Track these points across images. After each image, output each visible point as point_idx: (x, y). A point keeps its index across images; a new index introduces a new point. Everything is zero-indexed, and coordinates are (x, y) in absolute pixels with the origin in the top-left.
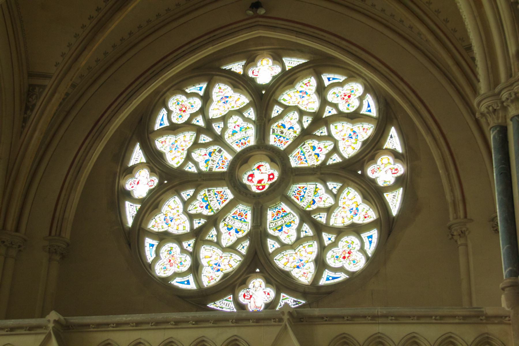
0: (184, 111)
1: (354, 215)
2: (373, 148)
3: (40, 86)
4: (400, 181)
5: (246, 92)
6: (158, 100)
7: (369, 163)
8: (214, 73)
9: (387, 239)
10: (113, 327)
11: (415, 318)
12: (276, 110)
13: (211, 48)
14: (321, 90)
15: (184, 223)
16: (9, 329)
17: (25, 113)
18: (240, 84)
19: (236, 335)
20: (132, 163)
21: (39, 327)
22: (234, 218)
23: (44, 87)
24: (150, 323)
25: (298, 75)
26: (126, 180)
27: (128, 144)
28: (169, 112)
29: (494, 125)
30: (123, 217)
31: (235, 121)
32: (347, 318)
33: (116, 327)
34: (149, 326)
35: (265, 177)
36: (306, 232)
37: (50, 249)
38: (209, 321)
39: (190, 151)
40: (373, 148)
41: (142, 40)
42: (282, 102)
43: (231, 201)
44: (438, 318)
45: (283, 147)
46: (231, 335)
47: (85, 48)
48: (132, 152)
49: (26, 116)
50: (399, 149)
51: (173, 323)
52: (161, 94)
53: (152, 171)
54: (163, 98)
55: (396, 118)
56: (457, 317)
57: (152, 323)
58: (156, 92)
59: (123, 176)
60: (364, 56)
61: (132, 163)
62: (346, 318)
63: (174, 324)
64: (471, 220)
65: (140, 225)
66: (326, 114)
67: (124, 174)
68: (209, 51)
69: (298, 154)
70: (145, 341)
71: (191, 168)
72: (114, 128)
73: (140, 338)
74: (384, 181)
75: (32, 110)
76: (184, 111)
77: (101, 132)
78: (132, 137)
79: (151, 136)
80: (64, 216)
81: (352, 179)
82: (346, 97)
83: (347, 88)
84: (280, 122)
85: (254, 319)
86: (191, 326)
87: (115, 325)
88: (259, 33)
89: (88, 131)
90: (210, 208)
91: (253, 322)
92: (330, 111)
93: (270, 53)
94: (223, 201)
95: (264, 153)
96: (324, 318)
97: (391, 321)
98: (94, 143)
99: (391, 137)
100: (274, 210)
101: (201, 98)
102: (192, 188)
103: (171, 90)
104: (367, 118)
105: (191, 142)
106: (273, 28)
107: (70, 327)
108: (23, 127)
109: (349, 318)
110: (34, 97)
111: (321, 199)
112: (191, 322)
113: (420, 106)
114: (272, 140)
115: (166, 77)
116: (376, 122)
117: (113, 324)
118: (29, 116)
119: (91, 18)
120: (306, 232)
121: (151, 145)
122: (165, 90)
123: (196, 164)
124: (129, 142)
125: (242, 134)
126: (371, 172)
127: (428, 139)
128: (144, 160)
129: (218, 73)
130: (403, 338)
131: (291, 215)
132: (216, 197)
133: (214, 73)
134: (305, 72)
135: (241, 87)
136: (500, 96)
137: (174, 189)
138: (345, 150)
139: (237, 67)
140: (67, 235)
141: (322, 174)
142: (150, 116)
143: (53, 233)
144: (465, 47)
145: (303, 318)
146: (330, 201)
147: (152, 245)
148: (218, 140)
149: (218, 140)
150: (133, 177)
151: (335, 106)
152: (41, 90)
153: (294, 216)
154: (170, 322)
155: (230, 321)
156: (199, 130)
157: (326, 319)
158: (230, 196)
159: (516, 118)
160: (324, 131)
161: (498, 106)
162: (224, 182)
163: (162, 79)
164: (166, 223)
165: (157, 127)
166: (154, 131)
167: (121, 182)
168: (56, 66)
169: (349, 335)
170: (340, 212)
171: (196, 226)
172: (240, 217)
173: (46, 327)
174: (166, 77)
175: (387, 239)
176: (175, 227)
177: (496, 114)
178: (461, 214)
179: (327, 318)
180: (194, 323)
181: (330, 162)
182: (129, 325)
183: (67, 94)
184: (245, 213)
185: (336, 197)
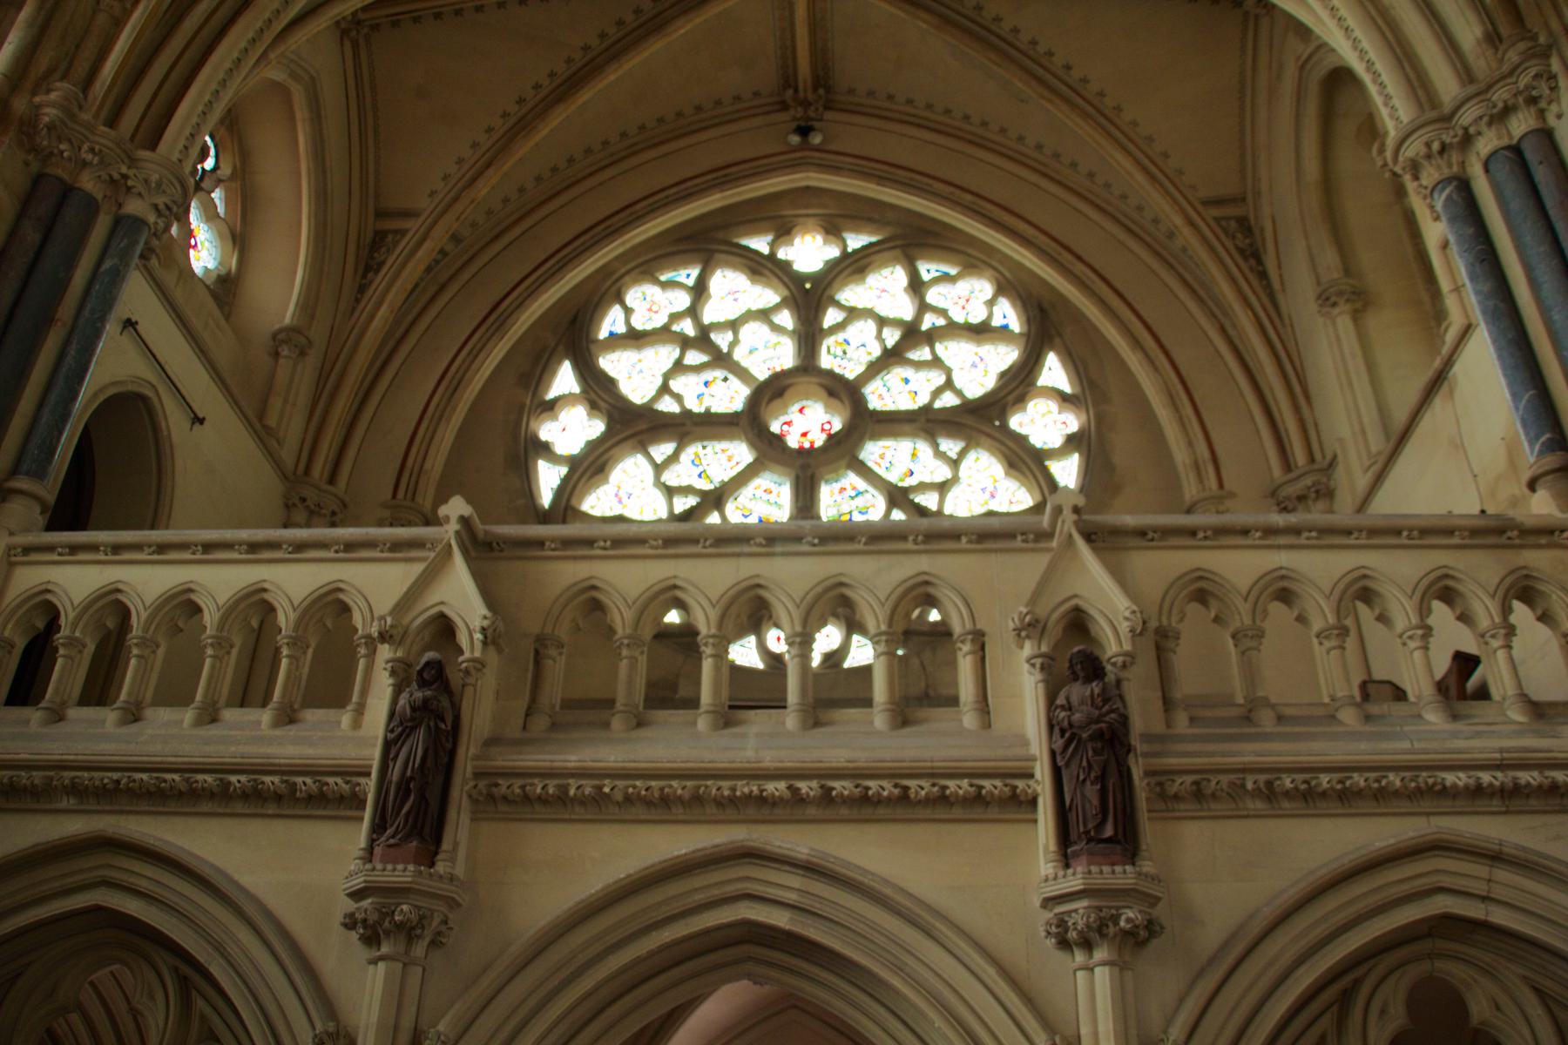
0: (656, 312)
3: (396, 232)
4: (1073, 442)
5: (776, 281)
10: (605, 548)
11: (1364, 534)
12: (831, 317)
13: (718, 196)
14: (916, 286)
17: (364, 276)
20: (552, 394)
21: (418, 544)
23: (403, 233)
24: (702, 541)
26: (543, 421)
27: (548, 360)
28: (628, 311)
29: (1440, 178)
30: (534, 487)
31: (753, 332)
32: (1205, 532)
39: (667, 377)
41: (591, 175)
42: (843, 302)
43: (749, 466)
44: (1415, 533)
45: (851, 375)
46: (910, 572)
47: (488, 165)
48: (554, 373)
49: (364, 281)
50: (1067, 388)
53: (593, 407)
54: (618, 284)
55: (1060, 335)
56: (1457, 533)
57: (706, 540)
61: (552, 394)
62: (1201, 535)
64: (1232, 495)
65: (568, 500)
66: (925, 326)
67: (539, 410)
68: (713, 202)
71: (667, 405)
72: (529, 317)
75: (377, 271)
76: (656, 312)
77: (504, 321)
78: (557, 346)
79: (593, 347)
80: (422, 467)
84: (840, 337)
86: (806, 548)
87: (609, 543)
88: (808, 178)
91: (970, 542)
92: (928, 321)
97: (1306, 542)
98: (488, 340)
102: (668, 440)
104: (1003, 333)
107: (495, 544)
108: (358, 301)
109: (1209, 533)
110: (384, 250)
113: (1115, 302)
114: (826, 361)
116: (1023, 341)
117: (605, 541)
118: (371, 282)
119: (505, 115)
123: (678, 398)
126: (1017, 422)
127: (1133, 360)
128: (576, 389)
130: (1340, 580)
134: (886, 255)
136: (1454, 122)
139: (760, 244)
141: (928, 421)
142: (592, 316)
145: (1096, 533)
146: (942, 472)
148: (721, 360)
149: (721, 360)
150: (555, 418)
151: (943, 312)
152: (399, 237)
156: (685, 343)
159: (1505, 152)
160: (923, 354)
161: (1455, 136)
163: (623, 243)
164: (620, 501)
165: (603, 334)
166: (597, 341)
167: (533, 424)
168: (430, 196)
177: (1445, 156)
178: (1212, 482)
179: (1155, 532)
180: (816, 541)
181: (938, 405)
185: (955, 464)
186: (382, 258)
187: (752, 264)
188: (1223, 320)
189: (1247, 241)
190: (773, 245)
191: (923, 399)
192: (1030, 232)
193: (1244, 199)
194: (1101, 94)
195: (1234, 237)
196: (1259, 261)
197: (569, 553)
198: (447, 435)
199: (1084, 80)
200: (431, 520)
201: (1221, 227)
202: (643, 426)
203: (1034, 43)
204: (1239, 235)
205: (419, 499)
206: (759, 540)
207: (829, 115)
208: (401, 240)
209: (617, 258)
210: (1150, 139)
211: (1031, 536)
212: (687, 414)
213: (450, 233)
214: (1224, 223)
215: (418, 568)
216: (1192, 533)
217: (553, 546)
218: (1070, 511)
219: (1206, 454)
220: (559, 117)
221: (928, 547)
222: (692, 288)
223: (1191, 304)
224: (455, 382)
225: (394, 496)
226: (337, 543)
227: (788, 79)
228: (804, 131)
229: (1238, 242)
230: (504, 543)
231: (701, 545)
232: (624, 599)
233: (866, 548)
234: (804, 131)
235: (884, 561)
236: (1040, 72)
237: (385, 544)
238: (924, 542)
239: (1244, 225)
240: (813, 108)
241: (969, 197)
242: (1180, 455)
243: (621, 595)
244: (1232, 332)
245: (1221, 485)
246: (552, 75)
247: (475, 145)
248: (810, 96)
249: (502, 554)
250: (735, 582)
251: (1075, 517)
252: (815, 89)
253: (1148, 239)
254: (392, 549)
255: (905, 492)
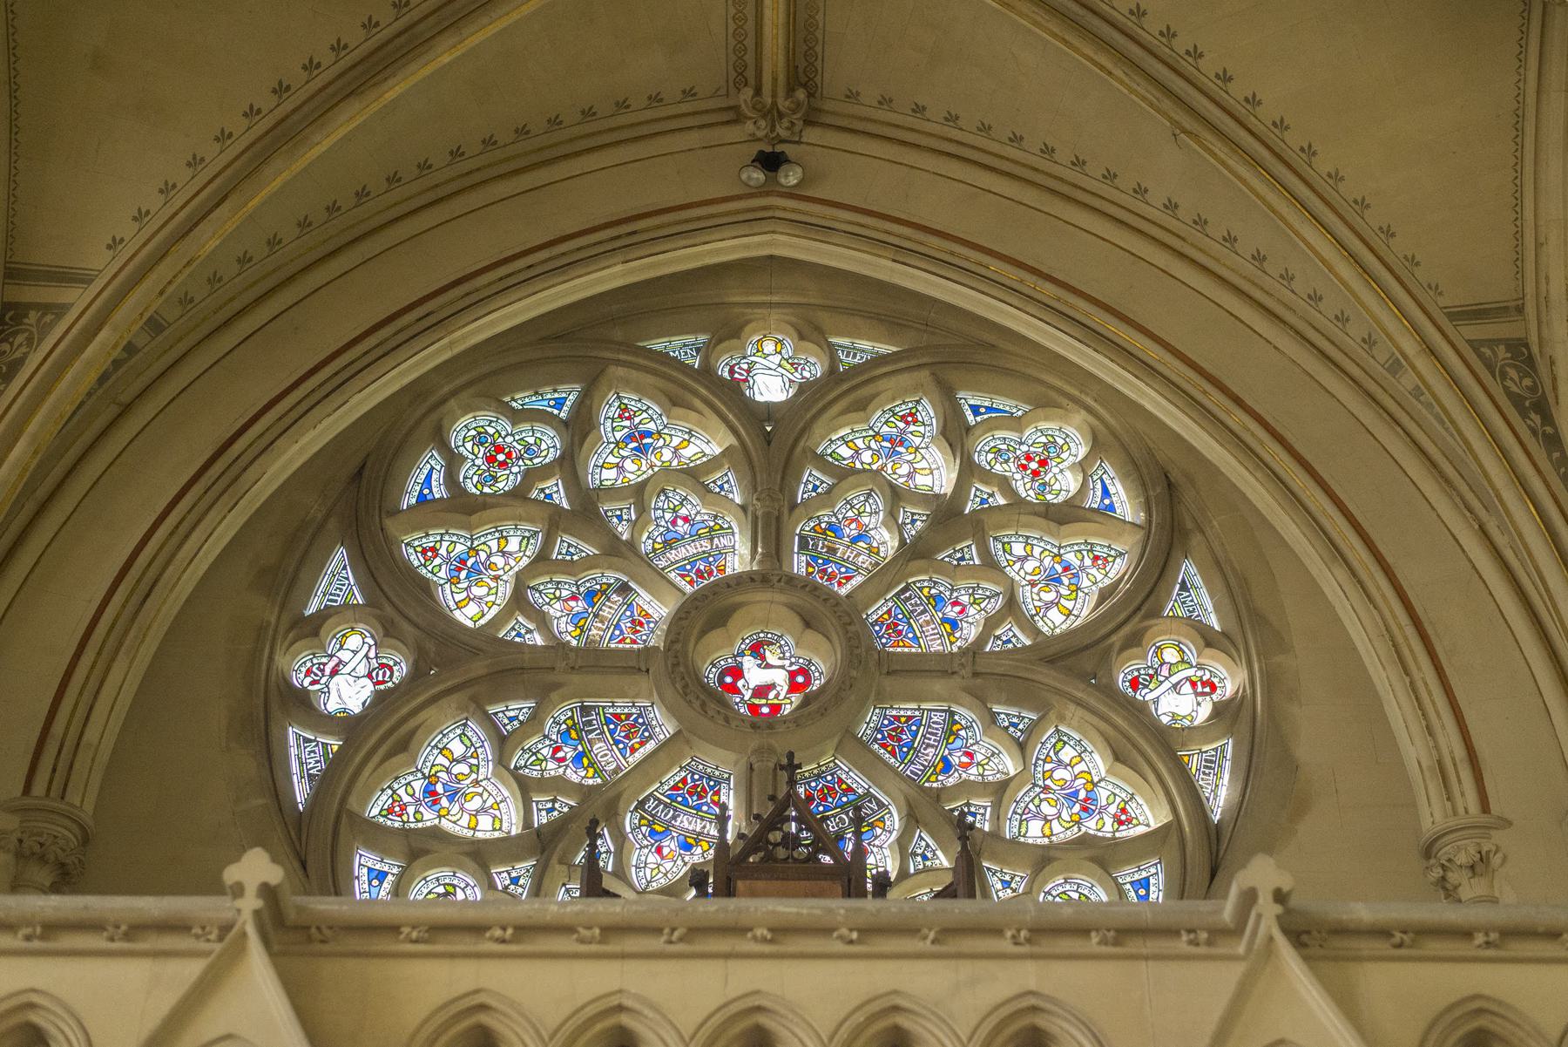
1: (1084, 815)
2: (1139, 609)
3: (45, 308)
6: (418, 422)
7: (1126, 654)
8: (608, 355)
9: (1209, 887)
10: (503, 941)
12: (812, 480)
14: (955, 434)
15: (495, 806)
16: (39, 930)
18: (696, 394)
19: (1031, 993)
22: (673, 801)
23: (60, 310)
24: (666, 931)
25: (882, 384)
28: (453, 461)
32: (1487, 934)
33: (514, 940)
34: (656, 944)
35: (780, 678)
36: (925, 858)
37: (20, 841)
38: (919, 931)
40: (1139, 609)
46: (1008, 992)
51: (765, 932)
52: (433, 399)
53: (388, 632)
55: (1203, 532)
57: (673, 930)
58: (416, 391)
59: (286, 643)
60: (1114, 328)
62: (1480, 938)
63: (769, 937)
64: (1506, 823)
65: (344, 800)
69: (886, 616)
70: (637, 997)
73: (620, 991)
74: (1173, 713)
81: (1079, 695)
82: (1034, 465)
83: (1034, 437)
85: (1109, 930)
86: (840, 947)
87: (510, 931)
89: (192, 471)
90: (591, 765)
91: (1104, 942)
93: (787, 318)
94: (637, 746)
95: (782, 598)
96: (1392, 936)
99: (1184, 587)
100: (813, 784)
101: (564, 426)
103: (464, 395)
105: (525, 558)
106: (822, 230)
109: (1493, 936)
110: (20, 339)
111: (972, 758)
112: (844, 931)
115: (464, 337)
117: (504, 929)
120: (925, 858)
121: (392, 554)
122: (446, 389)
123: (542, 621)
124: (314, 536)
125: (698, 546)
127: (1331, 582)
129: (622, 357)
131: (870, 801)
132: (612, 732)
133: (608, 355)
134: (905, 379)
135: (698, 403)
137: (469, 691)
138: (1041, 615)
139: (681, 346)
140: (84, 799)
143: (39, 788)
144: (1445, 311)
145: (1308, 932)
147: (381, 876)
152: (48, 318)
153: (881, 805)
154: (751, 929)
155: (1009, 934)
156: (555, 522)
157: (1402, 939)
158: (664, 725)
162: (644, 682)
169: (1500, 1003)
170: (1037, 801)
171: (541, 819)
172: (695, 798)
173: (203, 928)
174: (464, 337)
175: (1209, 887)
176: (464, 821)
178: (1472, 800)
179: (1405, 932)
180: (855, 935)
182: (575, 936)
183: (130, 349)
184: (712, 788)
186: (18, 355)
187: (671, 387)
188: (1482, 513)
189: (1527, 382)
190: (706, 351)
191: (970, 632)
192: (1153, 353)
193: (1520, 310)
194: (1280, 125)
195: (1504, 375)
196: (1548, 418)
197: (439, 948)
198: (125, 677)
199: (1253, 101)
200: (213, 886)
201: (1480, 356)
202: (479, 668)
203: (1169, 34)
204: (1513, 373)
205: (74, 797)
206: (759, 932)
207: (812, 135)
208: (52, 325)
209: (436, 369)
210: (1362, 204)
211: (1204, 936)
212: (558, 647)
213: (146, 316)
214: (1486, 351)
215: (192, 970)
216: (1466, 934)
217: (414, 935)
218: (1270, 898)
219: (1460, 752)
220: (349, 120)
221: (1036, 949)
222: (566, 423)
223: (1429, 487)
224: (144, 587)
225: (27, 790)
226: (29, 923)
227: (744, 73)
228: (771, 162)
229: (1509, 383)
230: (331, 928)
231: (665, 938)
232: (537, 1032)
233: (937, 948)
234: (771, 162)
235: (966, 968)
236: (1178, 85)
237: (118, 927)
238: (1029, 941)
239: (1523, 355)
240: (785, 123)
241: (1050, 288)
242: (1414, 751)
243: (530, 1022)
244: (1501, 540)
245: (1485, 807)
246: (338, 48)
247: (194, 162)
248: (784, 104)
249: (326, 948)
250: (722, 1001)
251: (1278, 909)
252: (790, 91)
253: (1356, 371)
254: (127, 937)
255: (938, 796)
